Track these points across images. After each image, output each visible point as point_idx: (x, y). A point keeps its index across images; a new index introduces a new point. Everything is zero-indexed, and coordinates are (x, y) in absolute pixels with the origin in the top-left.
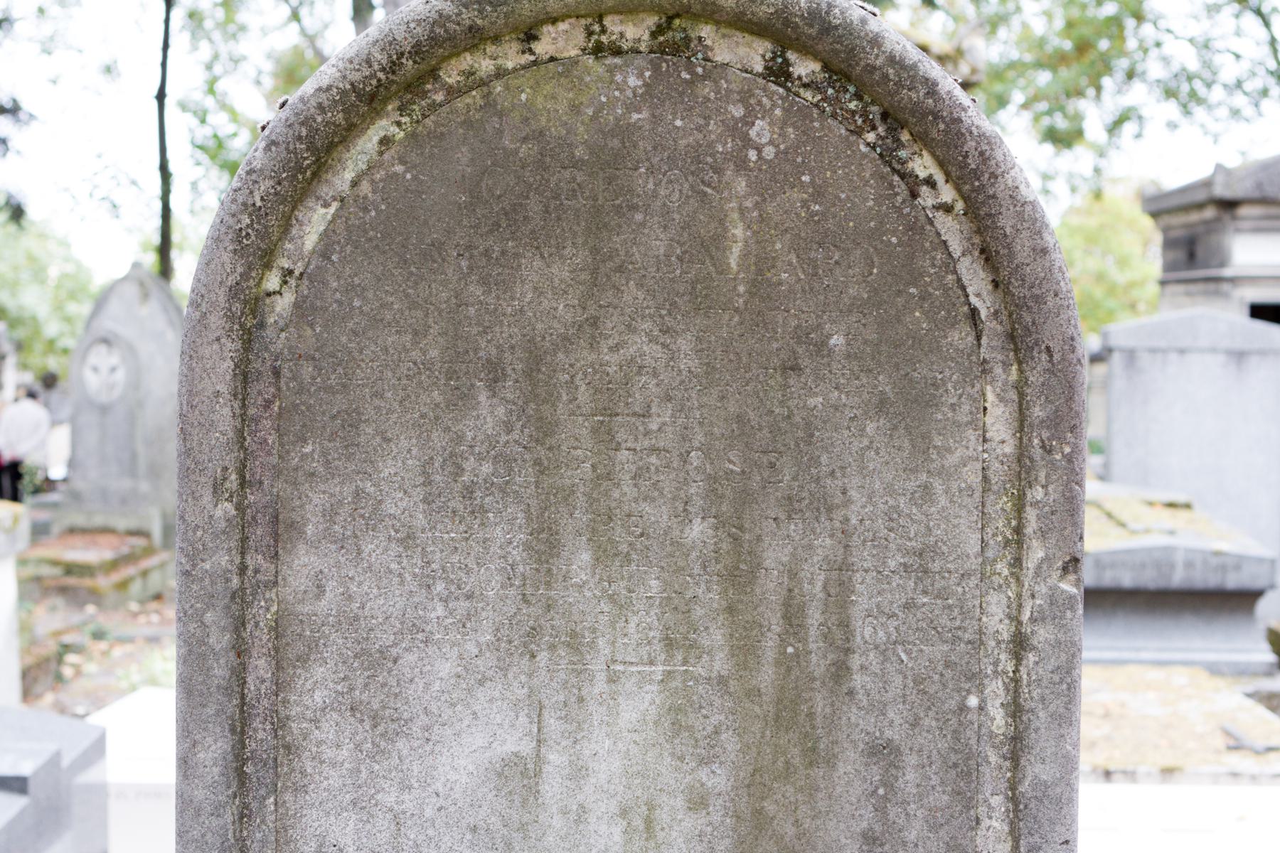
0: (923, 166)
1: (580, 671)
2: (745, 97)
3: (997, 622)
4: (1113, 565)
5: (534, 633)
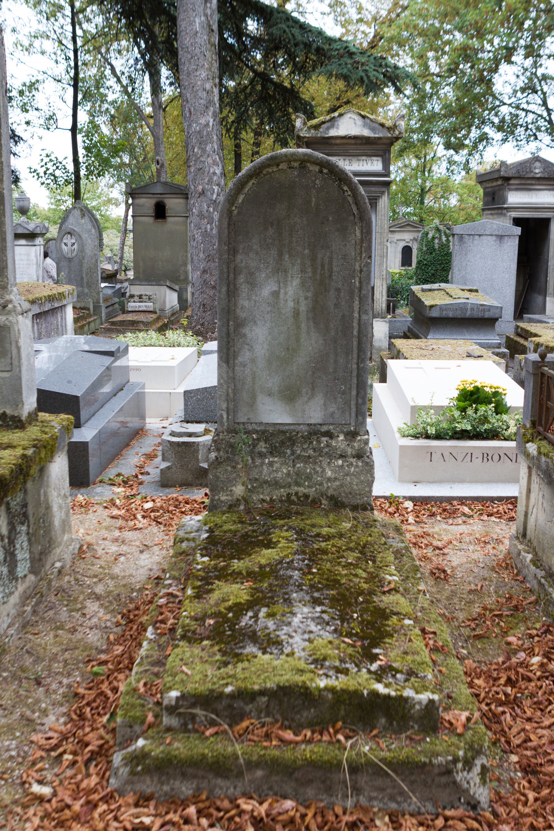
0: (345, 188)
1: (286, 276)
2: (315, 176)
3: (357, 267)
4: (446, 310)
5: (279, 269)
